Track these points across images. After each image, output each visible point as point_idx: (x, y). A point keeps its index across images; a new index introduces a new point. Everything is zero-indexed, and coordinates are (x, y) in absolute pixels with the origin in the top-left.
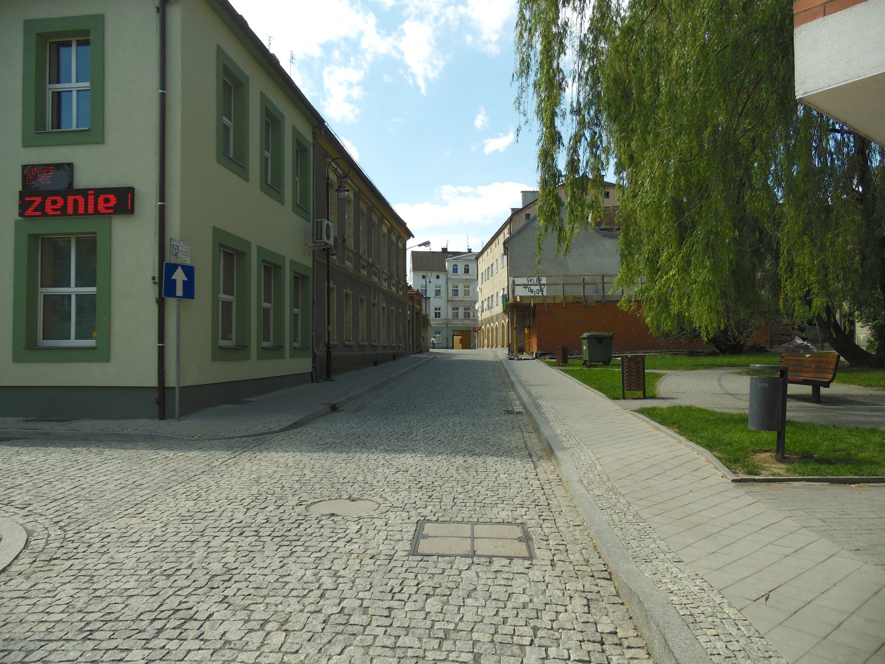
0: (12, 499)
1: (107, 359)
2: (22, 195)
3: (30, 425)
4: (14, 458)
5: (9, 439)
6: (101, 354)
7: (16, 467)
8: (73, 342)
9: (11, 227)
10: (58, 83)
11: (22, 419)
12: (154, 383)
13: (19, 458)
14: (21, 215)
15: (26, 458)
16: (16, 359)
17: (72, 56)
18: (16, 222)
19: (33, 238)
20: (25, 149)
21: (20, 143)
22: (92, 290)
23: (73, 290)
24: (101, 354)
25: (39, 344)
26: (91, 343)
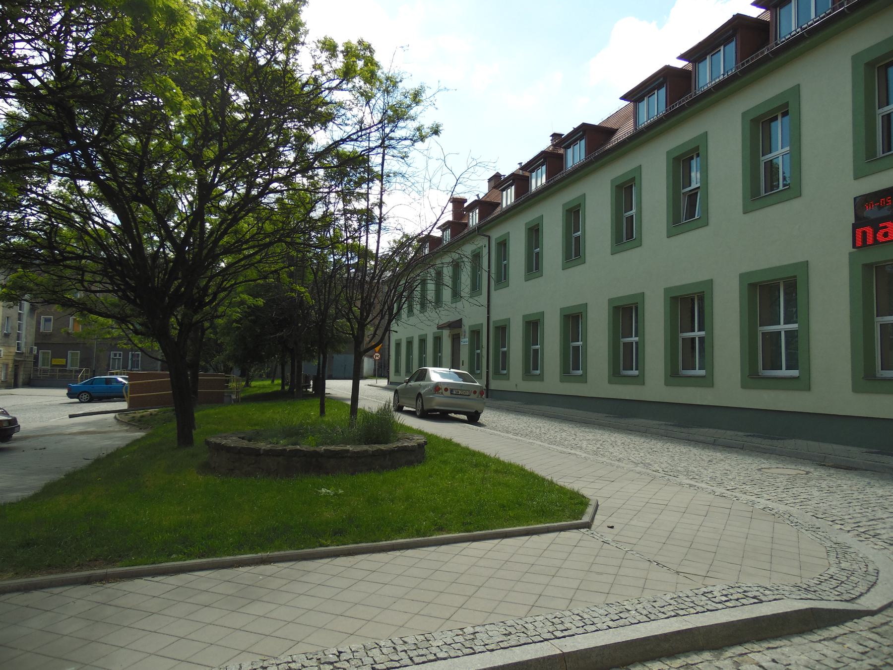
0: (878, 532)
1: (712, 385)
2: (855, 227)
3: (875, 457)
4: (868, 490)
5: (856, 469)
6: (803, 384)
7: (873, 500)
8: (784, 372)
9: (846, 260)
10: (888, 104)
11: (865, 450)
12: (363, 383)
13: (872, 490)
14: (854, 246)
15: (880, 492)
16: (744, 386)
17: (778, 129)
18: (850, 254)
19: (867, 267)
20: (856, 182)
21: (852, 178)
22: (794, 326)
23: (782, 327)
24: (803, 384)
25: (878, 375)
26: (795, 373)
